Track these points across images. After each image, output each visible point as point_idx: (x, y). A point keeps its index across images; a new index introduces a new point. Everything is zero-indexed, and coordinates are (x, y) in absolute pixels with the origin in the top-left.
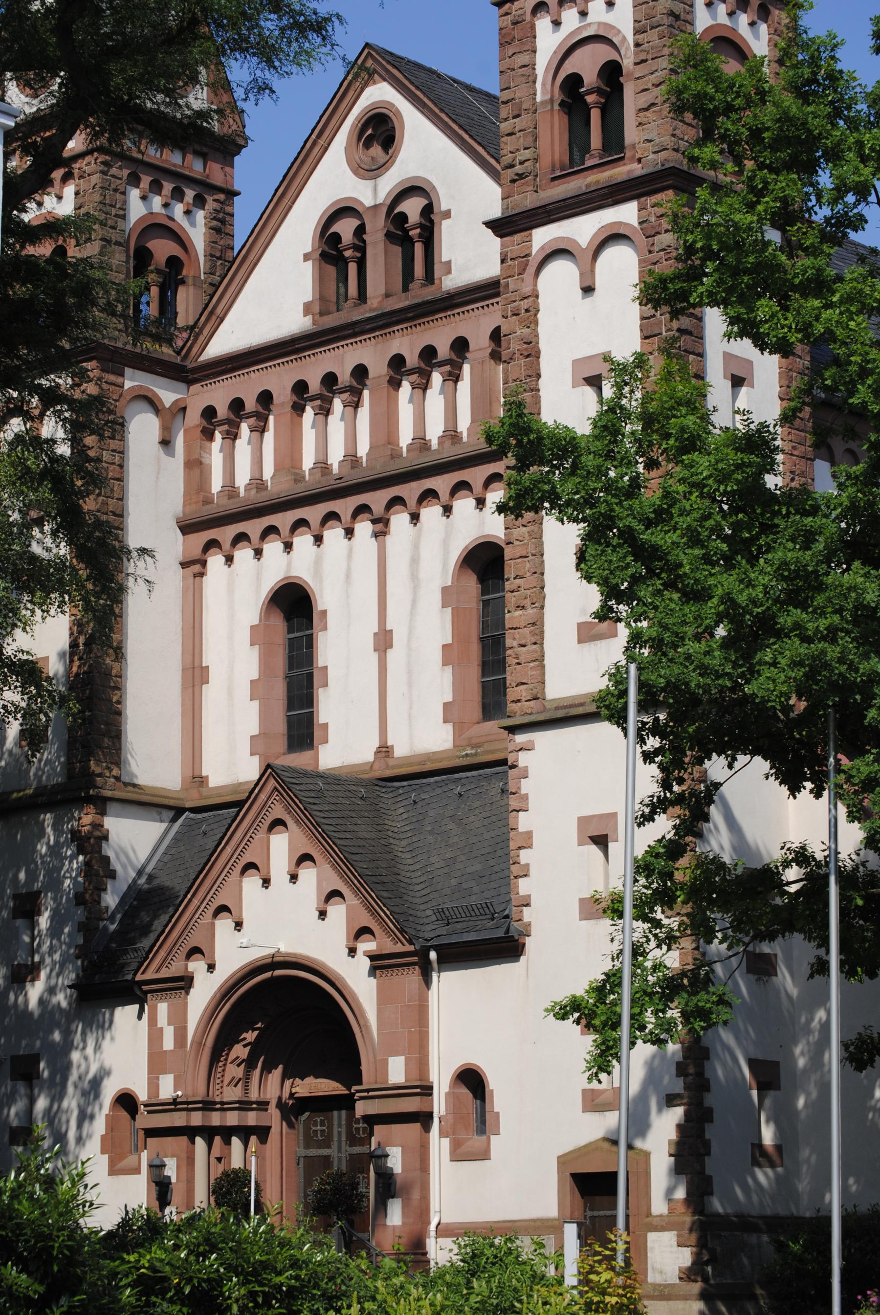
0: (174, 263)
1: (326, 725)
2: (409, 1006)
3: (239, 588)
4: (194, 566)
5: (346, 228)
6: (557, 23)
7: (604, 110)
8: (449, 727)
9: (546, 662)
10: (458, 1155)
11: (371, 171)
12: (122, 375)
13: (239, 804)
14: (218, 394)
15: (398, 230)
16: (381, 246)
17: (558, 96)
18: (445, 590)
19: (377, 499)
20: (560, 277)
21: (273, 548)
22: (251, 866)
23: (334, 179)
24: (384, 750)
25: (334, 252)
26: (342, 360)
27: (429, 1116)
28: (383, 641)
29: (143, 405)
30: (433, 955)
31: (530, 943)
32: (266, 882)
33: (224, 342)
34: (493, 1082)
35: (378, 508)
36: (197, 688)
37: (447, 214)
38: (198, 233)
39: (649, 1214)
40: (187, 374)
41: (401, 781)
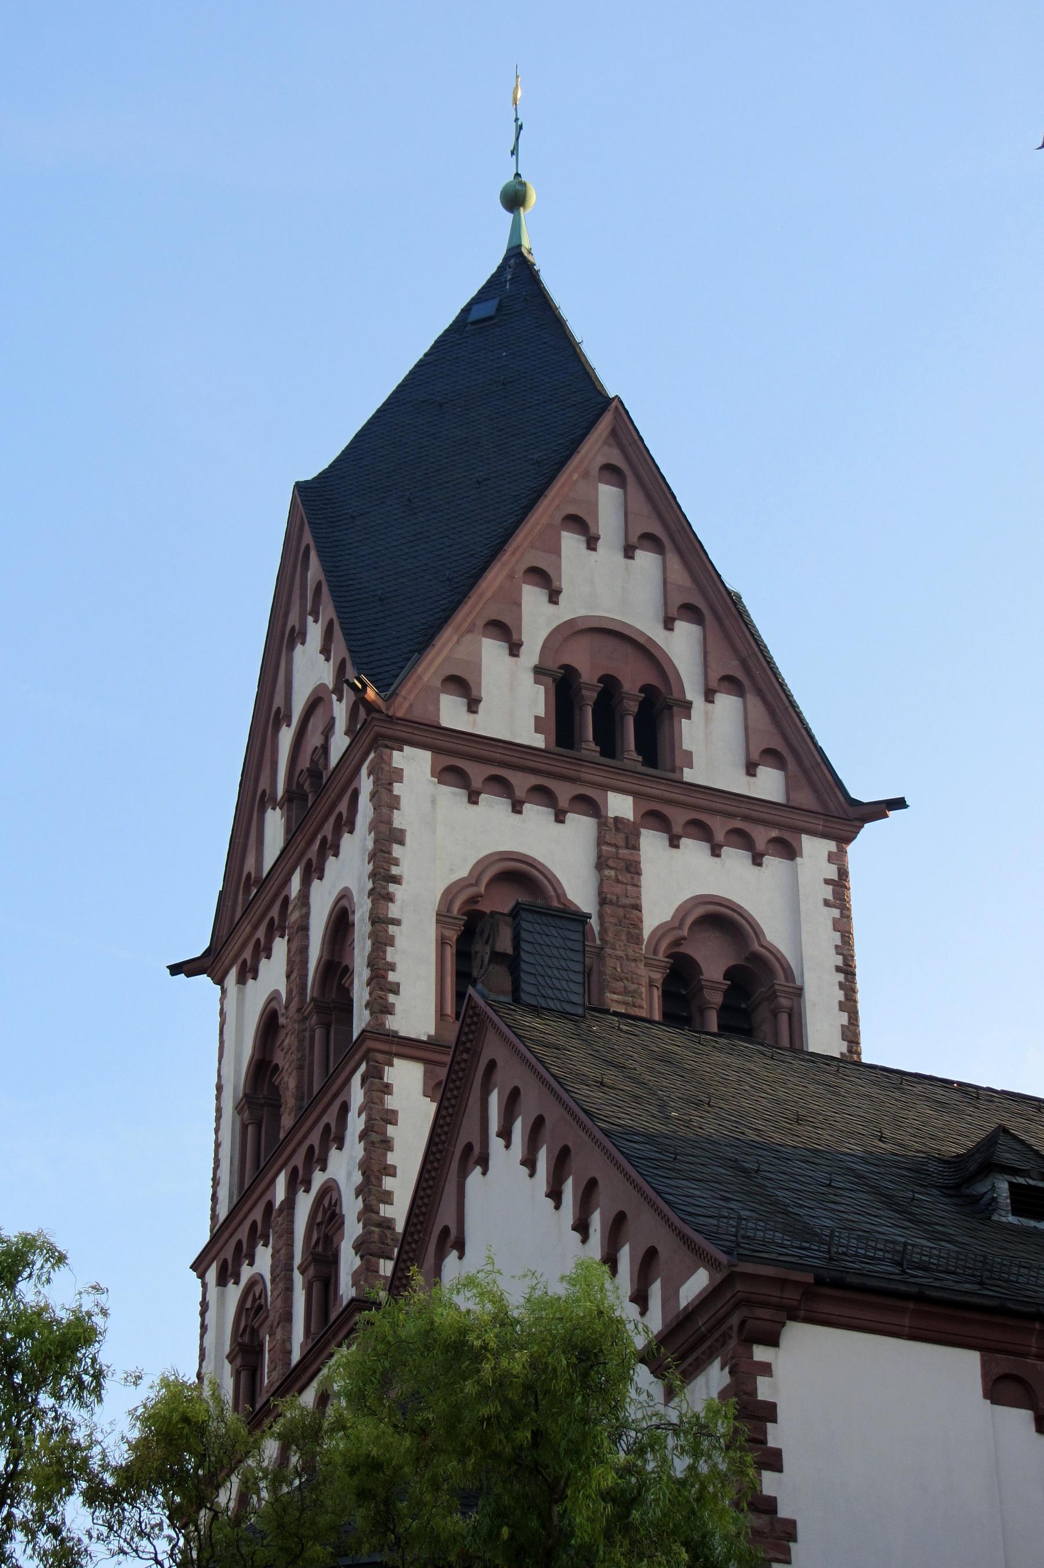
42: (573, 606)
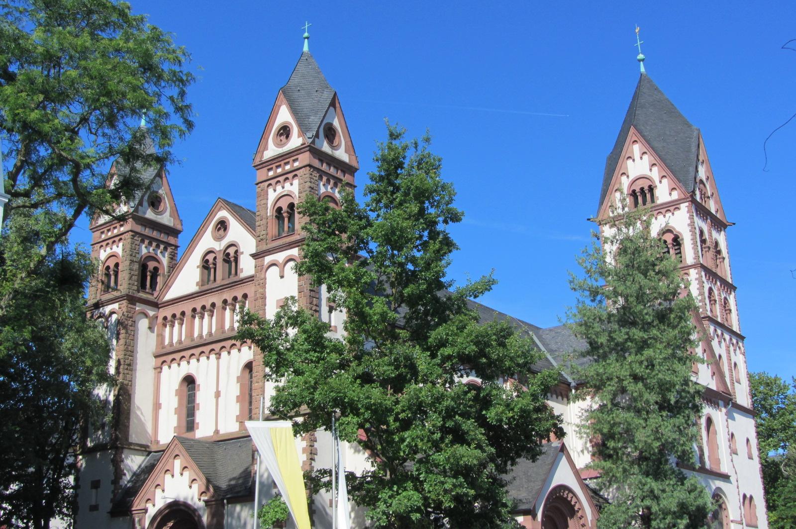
0: (156, 269)
1: (198, 423)
3: (173, 375)
4: (159, 369)
5: (210, 257)
6: (275, 190)
7: (289, 219)
8: (238, 423)
11: (219, 239)
12: (135, 305)
13: (164, 451)
14: (167, 312)
15: (227, 259)
16: (221, 264)
17: (275, 214)
18: (238, 378)
19: (217, 347)
20: (274, 272)
21: (184, 363)
23: (207, 242)
24: (217, 432)
25: (206, 266)
26: (207, 301)
28: (218, 394)
29: (143, 316)
30: (225, 501)
32: (173, 476)
33: (171, 295)
35: (217, 350)
37: (242, 253)
38: (165, 260)
40: (156, 305)
41: (222, 442)
42: (632, 177)
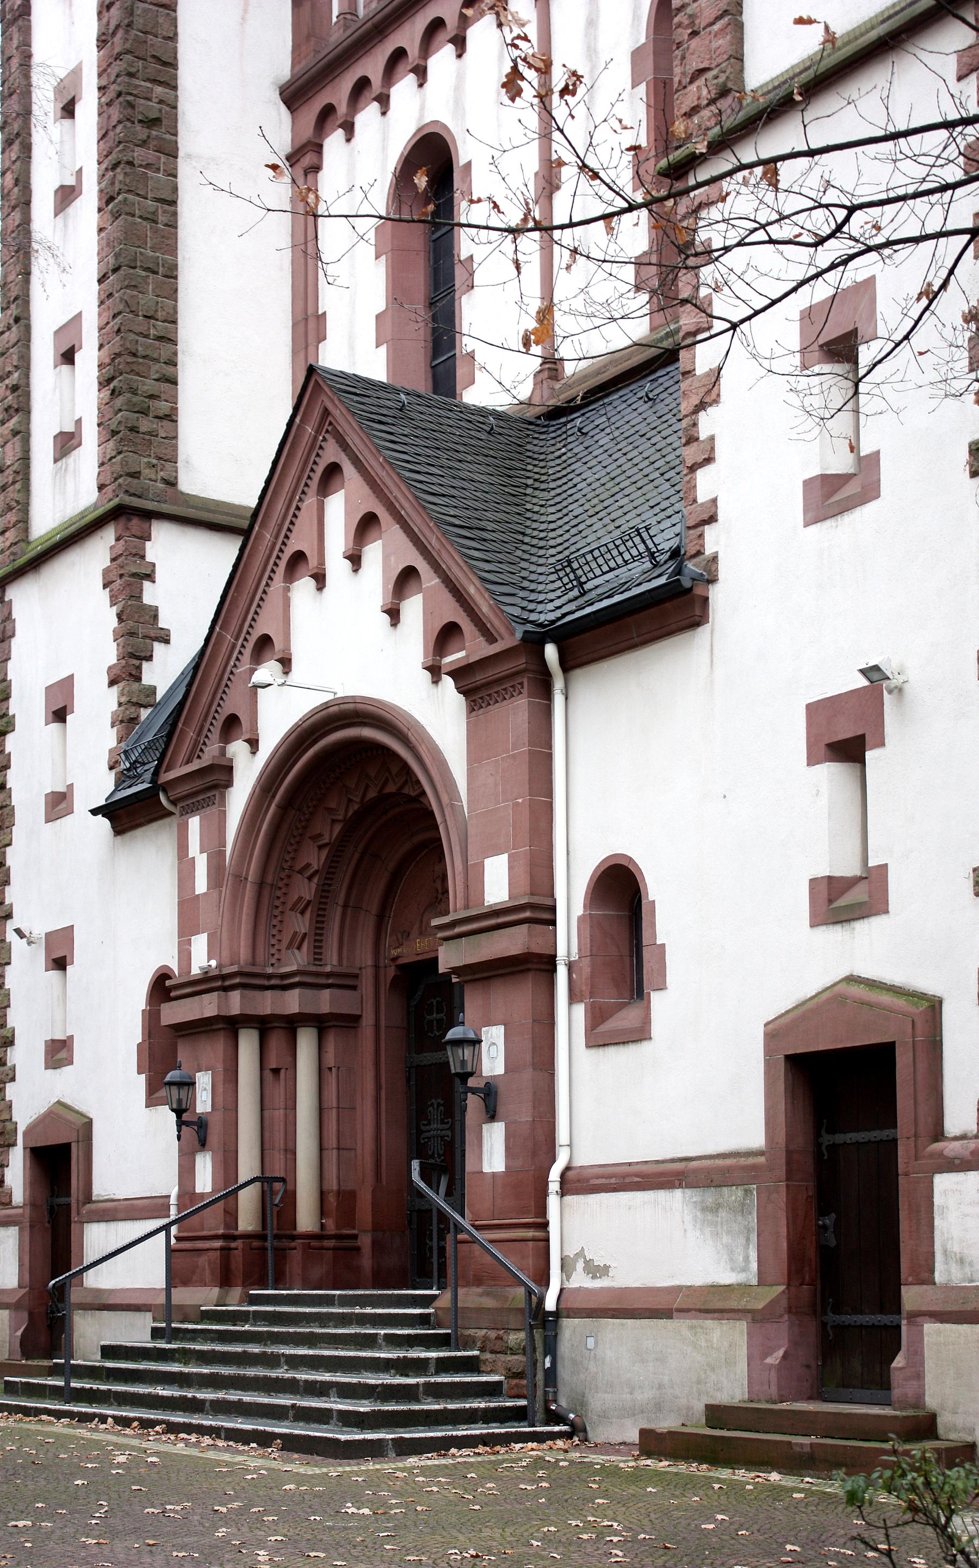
2: (514, 757)
9: (746, 18)
10: (601, 1035)
22: (299, 557)
27: (550, 962)
30: (551, 652)
31: (719, 596)
34: (657, 888)
36: (311, 349)
39: (938, 1133)
